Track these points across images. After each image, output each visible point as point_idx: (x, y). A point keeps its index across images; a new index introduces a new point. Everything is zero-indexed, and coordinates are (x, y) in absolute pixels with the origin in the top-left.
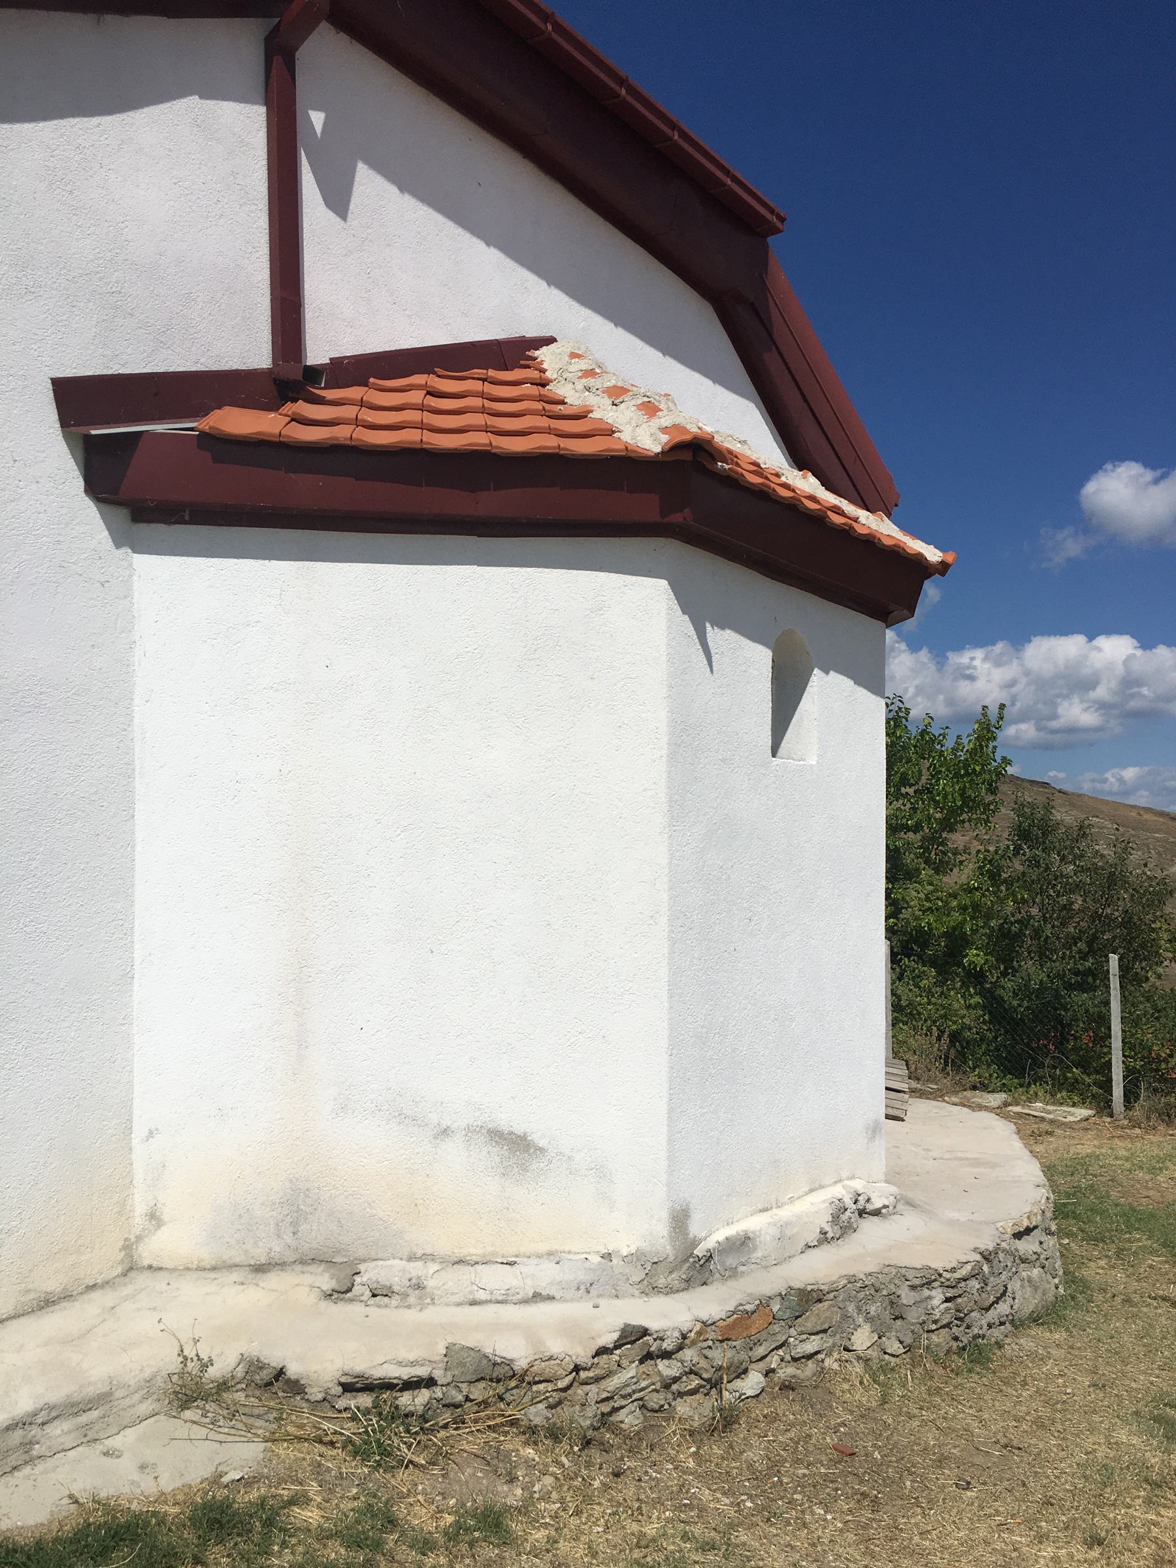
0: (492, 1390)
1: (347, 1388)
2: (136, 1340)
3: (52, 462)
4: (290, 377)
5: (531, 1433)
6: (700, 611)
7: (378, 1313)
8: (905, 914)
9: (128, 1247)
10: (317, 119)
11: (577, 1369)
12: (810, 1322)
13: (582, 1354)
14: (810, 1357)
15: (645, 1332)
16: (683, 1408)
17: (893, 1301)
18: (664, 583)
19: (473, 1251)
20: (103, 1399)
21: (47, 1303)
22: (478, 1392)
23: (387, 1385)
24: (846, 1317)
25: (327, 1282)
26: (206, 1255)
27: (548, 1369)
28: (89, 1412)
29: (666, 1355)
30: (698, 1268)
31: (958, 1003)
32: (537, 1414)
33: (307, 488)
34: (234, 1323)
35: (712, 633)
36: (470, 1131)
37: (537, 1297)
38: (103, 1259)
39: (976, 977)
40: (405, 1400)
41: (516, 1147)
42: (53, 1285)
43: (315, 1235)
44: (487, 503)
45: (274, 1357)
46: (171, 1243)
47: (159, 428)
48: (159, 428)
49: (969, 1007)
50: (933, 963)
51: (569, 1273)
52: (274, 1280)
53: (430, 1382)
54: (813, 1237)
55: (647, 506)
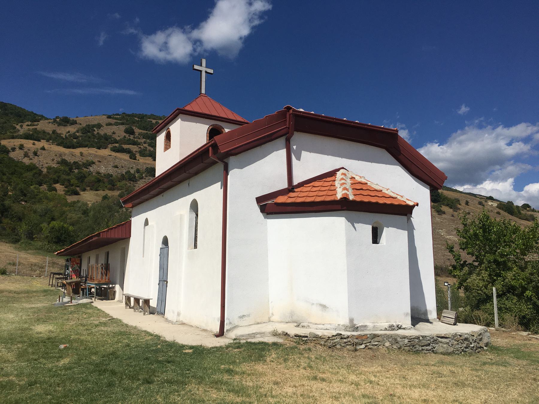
0: (317, 338)
1: (295, 336)
2: (269, 328)
3: (256, 208)
4: (291, 188)
5: (321, 345)
6: (352, 221)
7: (302, 329)
8: (507, 280)
9: (269, 318)
10: (295, 147)
11: (329, 337)
12: (376, 339)
13: (330, 336)
14: (376, 345)
15: (341, 334)
16: (348, 347)
17: (396, 340)
18: (344, 218)
19: (318, 323)
20: (264, 333)
21: (258, 323)
22: (314, 339)
23: (301, 336)
24: (384, 340)
25: (296, 324)
26: (280, 320)
27: (324, 337)
28: (262, 334)
29: (345, 338)
30: (356, 329)
31: (524, 307)
32: (323, 343)
33: (289, 209)
34: (281, 328)
35: (356, 225)
36: (317, 304)
37: (327, 329)
38: (266, 319)
39: (529, 299)
40: (303, 339)
41: (324, 307)
42: (259, 321)
43: (295, 318)
44: (315, 208)
45: (286, 331)
46: (275, 318)
47: (269, 202)
48: (269, 202)
49: (528, 308)
50: (517, 295)
51: (333, 327)
52: (288, 324)
53: (307, 337)
54: (383, 329)
55: (339, 207)
